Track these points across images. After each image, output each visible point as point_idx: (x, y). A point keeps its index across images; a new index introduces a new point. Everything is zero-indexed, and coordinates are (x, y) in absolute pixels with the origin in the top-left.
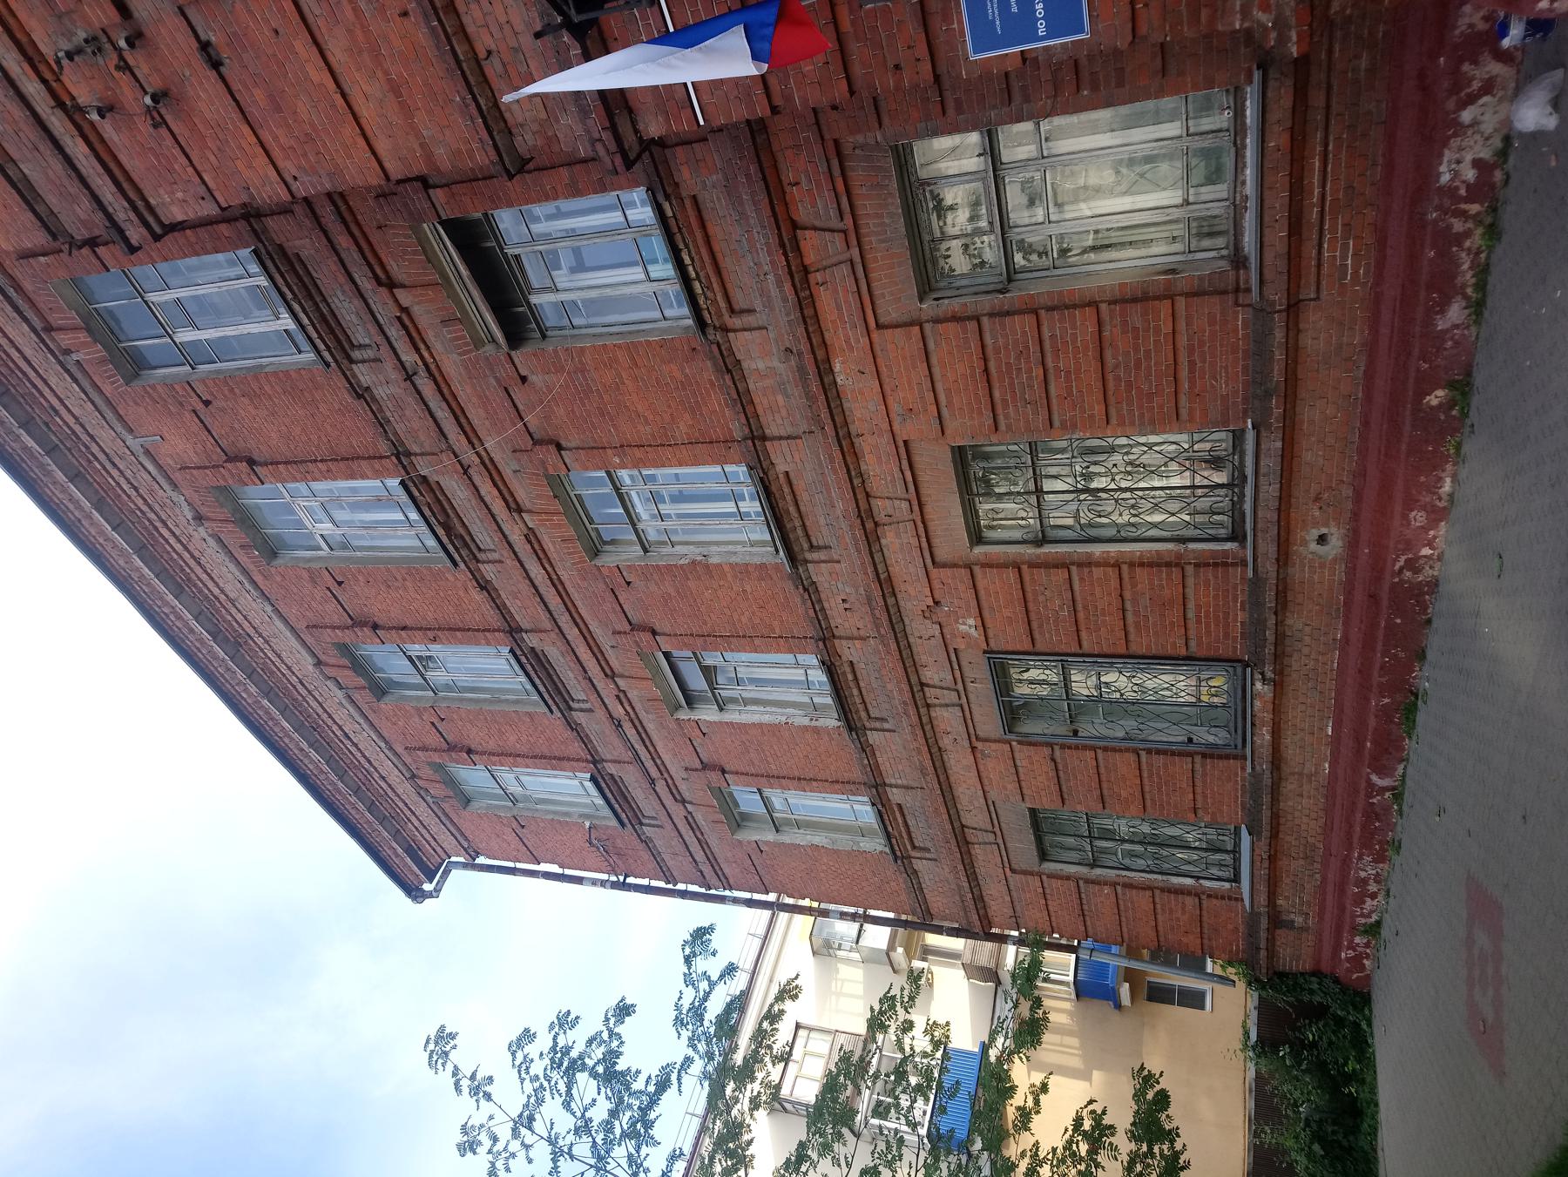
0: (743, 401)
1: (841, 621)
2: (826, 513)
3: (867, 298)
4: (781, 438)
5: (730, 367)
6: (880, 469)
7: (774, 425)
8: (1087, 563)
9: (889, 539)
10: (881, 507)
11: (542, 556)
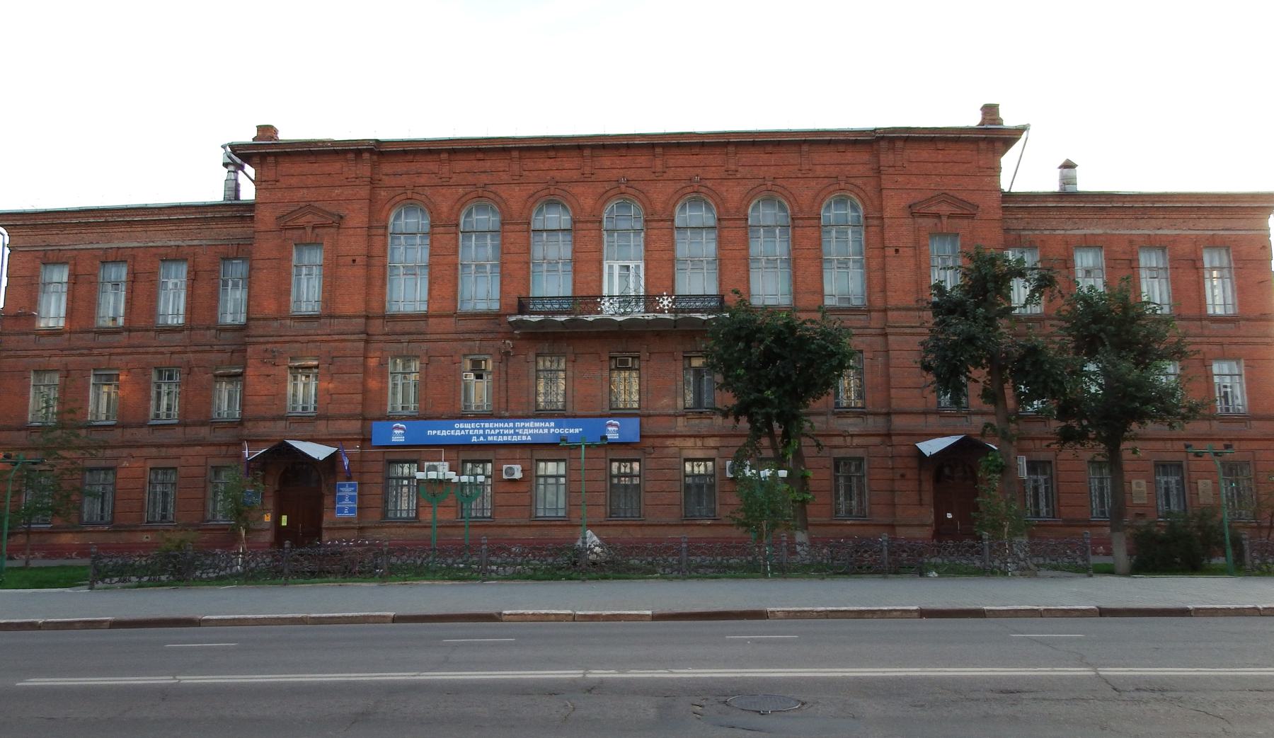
0: (194, 424)
1: (128, 432)
2: (159, 437)
3: (213, 456)
4: (887, 365)
5: (203, 424)
6: (174, 451)
7: (188, 429)
8: (144, 492)
9: (154, 450)
10: (164, 450)
11: (156, 353)
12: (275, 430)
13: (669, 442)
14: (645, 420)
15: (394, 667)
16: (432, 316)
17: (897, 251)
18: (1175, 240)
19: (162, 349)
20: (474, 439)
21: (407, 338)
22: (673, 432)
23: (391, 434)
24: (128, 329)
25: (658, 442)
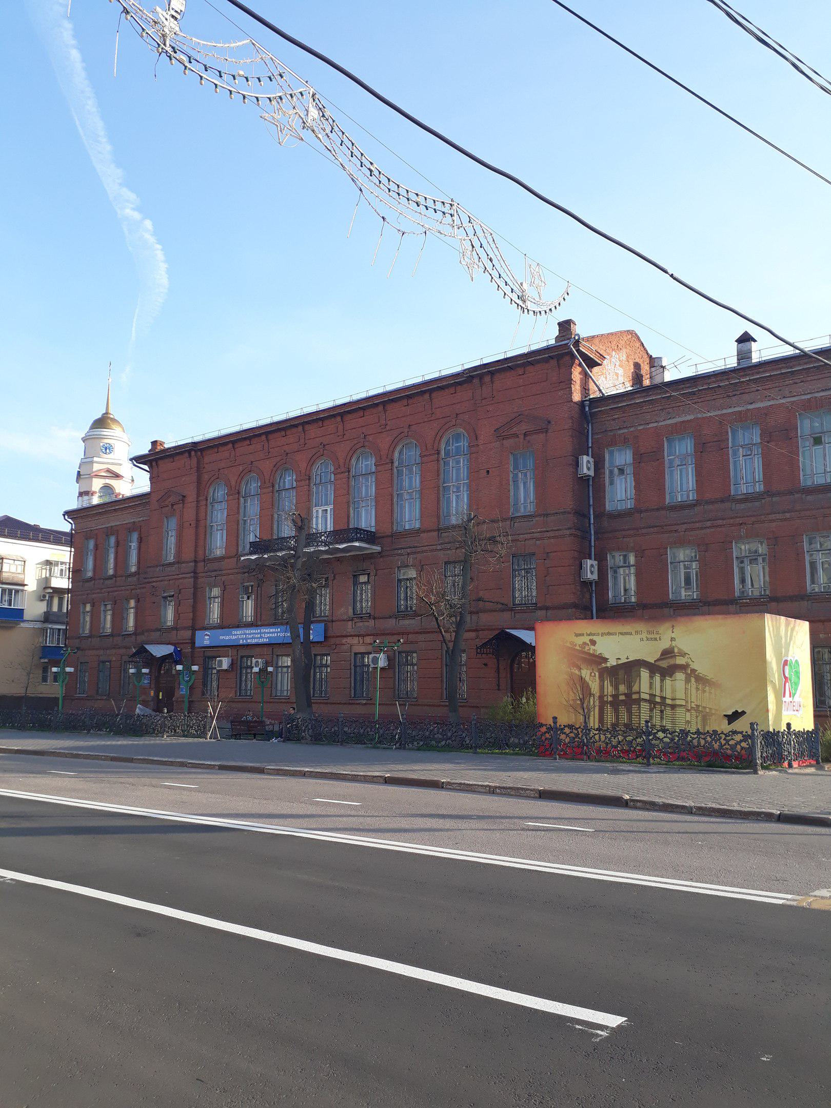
12: (500, 620)
13: (344, 640)
14: (330, 624)
15: (677, 874)
16: (424, 532)
17: (488, 472)
18: (765, 413)
19: (675, 528)
20: (241, 642)
21: (214, 574)
22: (344, 633)
23: (204, 639)
24: (768, 493)
25: (338, 640)
